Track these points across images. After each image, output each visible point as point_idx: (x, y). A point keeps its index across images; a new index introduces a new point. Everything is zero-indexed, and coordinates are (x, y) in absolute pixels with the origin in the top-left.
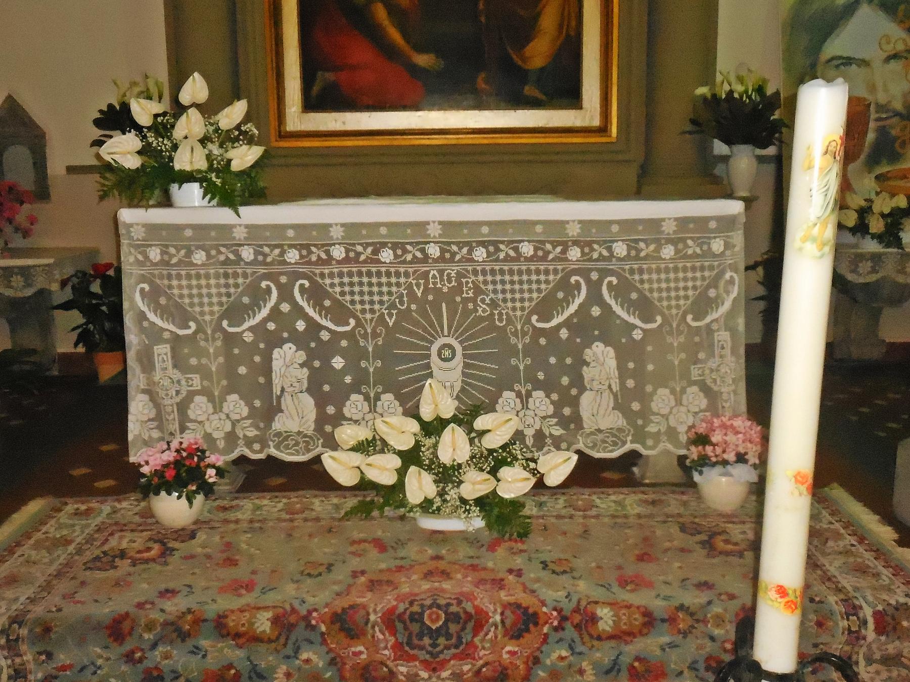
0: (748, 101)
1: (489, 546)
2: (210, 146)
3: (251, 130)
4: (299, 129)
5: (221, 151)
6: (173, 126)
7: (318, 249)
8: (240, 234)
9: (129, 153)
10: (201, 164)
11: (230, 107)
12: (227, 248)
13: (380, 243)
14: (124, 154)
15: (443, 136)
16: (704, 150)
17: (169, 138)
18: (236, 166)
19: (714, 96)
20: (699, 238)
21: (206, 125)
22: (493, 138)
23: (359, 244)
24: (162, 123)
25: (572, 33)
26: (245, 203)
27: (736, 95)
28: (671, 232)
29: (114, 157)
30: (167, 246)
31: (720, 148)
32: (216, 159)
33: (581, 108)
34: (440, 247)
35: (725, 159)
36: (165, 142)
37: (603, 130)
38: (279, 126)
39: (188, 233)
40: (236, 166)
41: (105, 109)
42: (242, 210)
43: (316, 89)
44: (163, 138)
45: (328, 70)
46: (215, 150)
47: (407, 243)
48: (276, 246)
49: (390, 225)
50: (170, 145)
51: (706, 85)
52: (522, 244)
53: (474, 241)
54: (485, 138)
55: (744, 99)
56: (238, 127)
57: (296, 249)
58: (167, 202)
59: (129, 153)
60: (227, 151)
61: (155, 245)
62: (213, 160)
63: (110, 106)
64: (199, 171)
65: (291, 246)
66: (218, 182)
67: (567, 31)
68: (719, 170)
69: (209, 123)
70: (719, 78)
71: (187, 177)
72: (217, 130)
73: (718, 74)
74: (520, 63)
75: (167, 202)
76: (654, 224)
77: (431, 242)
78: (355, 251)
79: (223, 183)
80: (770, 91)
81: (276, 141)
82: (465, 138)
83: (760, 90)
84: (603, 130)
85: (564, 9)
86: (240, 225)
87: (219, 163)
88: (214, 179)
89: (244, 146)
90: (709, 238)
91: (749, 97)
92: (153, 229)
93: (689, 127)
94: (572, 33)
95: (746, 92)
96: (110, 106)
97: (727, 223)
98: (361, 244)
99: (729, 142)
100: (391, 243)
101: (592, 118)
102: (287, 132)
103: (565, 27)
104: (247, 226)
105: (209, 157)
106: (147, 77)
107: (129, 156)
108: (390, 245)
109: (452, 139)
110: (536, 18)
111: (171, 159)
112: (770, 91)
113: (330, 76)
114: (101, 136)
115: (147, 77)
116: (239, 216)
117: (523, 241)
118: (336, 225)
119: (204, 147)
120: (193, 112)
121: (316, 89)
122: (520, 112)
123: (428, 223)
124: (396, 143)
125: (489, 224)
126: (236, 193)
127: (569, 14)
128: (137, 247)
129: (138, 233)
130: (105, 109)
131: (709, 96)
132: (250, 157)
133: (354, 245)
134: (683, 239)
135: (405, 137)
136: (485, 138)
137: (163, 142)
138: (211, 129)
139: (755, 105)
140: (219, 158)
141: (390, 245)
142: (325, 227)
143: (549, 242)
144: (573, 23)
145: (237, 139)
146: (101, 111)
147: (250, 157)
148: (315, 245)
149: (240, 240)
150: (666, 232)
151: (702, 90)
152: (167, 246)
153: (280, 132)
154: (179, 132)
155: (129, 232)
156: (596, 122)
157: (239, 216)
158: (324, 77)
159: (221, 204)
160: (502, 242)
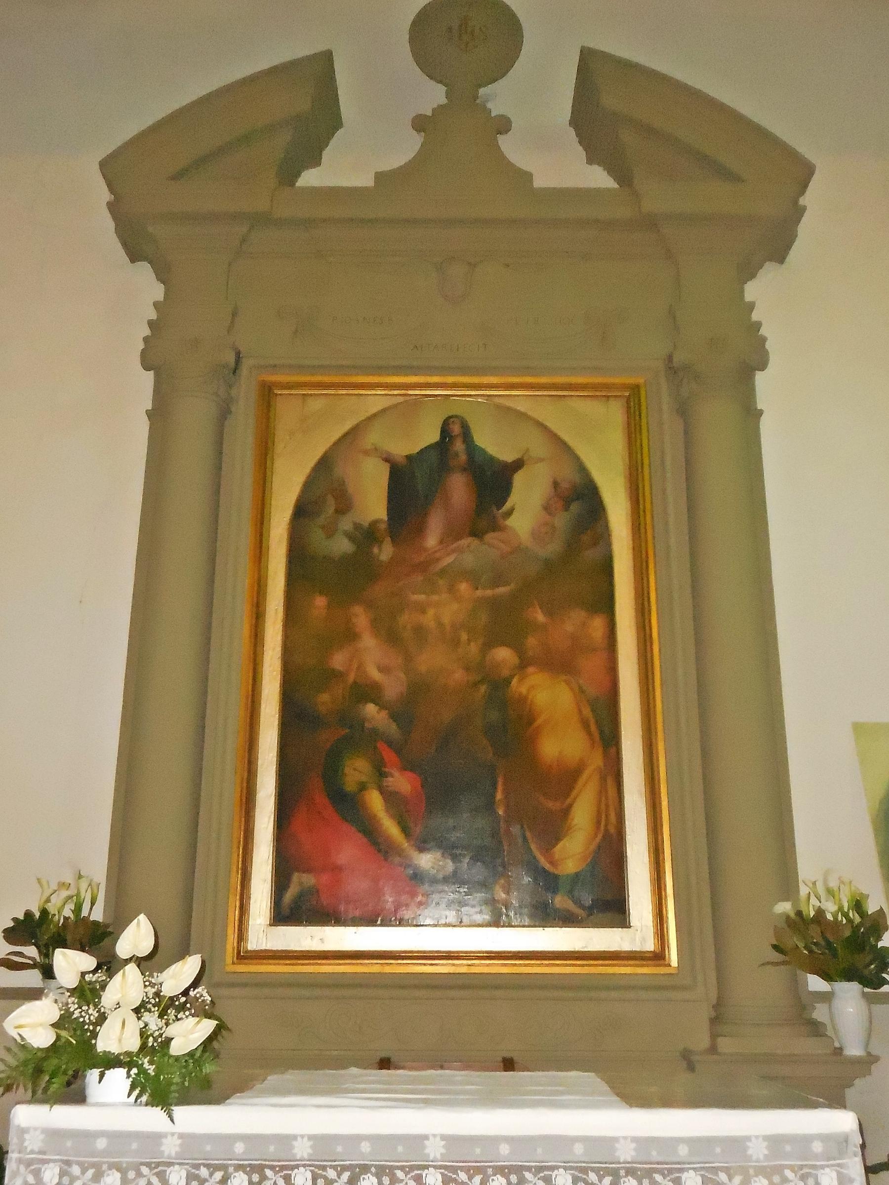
0: (844, 921)
1: (547, 889)
2: (147, 1017)
3: (202, 996)
4: (263, 948)
5: (161, 1023)
6: (103, 987)
7: (276, 1173)
8: (170, 1148)
9: (41, 1025)
10: (133, 1043)
11: (180, 963)
12: (151, 1169)
13: (359, 1166)
14: (33, 1026)
15: (450, 962)
16: (796, 987)
17: (96, 1006)
18: (177, 1048)
19: (799, 913)
20: (801, 1167)
21: (145, 986)
22: (515, 965)
23: (331, 1167)
24: (90, 983)
25: (612, 830)
26: (186, 1100)
27: (829, 917)
28: (761, 1157)
29: (21, 1031)
30: (68, 1163)
31: (816, 983)
32: (152, 1035)
33: (630, 927)
34: (442, 1174)
35: (826, 997)
36: (90, 1011)
37: (658, 957)
38: (239, 943)
39: (101, 1144)
40: (177, 1048)
41: (21, 917)
42: (179, 1111)
43: (289, 896)
44: (88, 1006)
45: (308, 870)
46: (152, 1020)
47: (398, 1168)
48: (217, 1168)
49: (375, 1139)
50: (97, 1015)
51: (787, 900)
52: (556, 1172)
53: (490, 1167)
54: (505, 965)
55: (840, 919)
56: (185, 993)
57: (245, 1172)
58: (79, 1098)
59: (41, 1025)
60: (167, 1024)
61: (54, 1161)
62: (147, 1038)
63: (28, 914)
64: (128, 1054)
65: (239, 1168)
66: (151, 1070)
67: (606, 826)
68: (820, 1013)
69: (150, 982)
70: (804, 891)
71: (110, 1062)
72: (157, 994)
73: (802, 886)
74: (547, 866)
75: (79, 1098)
76: (736, 1144)
77: (430, 1166)
78: (325, 1178)
79: (158, 1072)
80: (871, 908)
81: (233, 963)
82: (478, 965)
83: (858, 905)
84: (658, 957)
85: (600, 802)
86: (173, 1134)
87: (155, 1040)
88: (146, 1066)
89: (191, 1018)
90: (814, 1167)
91: (845, 915)
92: (55, 1135)
93: (777, 956)
94: (612, 830)
95: (841, 909)
96: (28, 914)
97: (839, 1142)
98: (334, 1168)
99: (827, 977)
100: (376, 1166)
101: (644, 940)
102: (247, 952)
103: (603, 823)
104: (181, 1136)
105: (144, 1034)
106: (80, 877)
107: (40, 1029)
108: (373, 1170)
109: (461, 967)
110: (566, 812)
111: (95, 1035)
112: (871, 908)
113: (309, 880)
114: (8, 954)
115: (80, 877)
116: (172, 1121)
117: (557, 1168)
118: (302, 1136)
119: (139, 1019)
120: (131, 969)
121: (289, 896)
122: (549, 930)
123: (426, 1137)
124: (388, 969)
125: (510, 1140)
126: (173, 1088)
127: (607, 806)
128: (29, 1163)
129: (33, 1142)
130: (21, 917)
131: (792, 915)
132: (196, 1035)
133: (324, 1168)
134: (779, 1170)
135: (399, 961)
136: (505, 965)
137: (87, 1012)
138: (151, 991)
139: (855, 929)
140: (157, 1033)
141: (373, 1170)
142: (285, 1140)
143: (593, 1170)
144: (613, 818)
145: (182, 1008)
146: (15, 920)
147: (196, 1035)
148: (272, 1168)
149: (169, 1157)
150: (754, 1158)
151: (784, 907)
152: (68, 1163)
153: (239, 952)
154: (108, 998)
155: (22, 1140)
156: (650, 946)
157: (172, 1121)
158: (300, 881)
159: (152, 1102)
160: (529, 1169)
